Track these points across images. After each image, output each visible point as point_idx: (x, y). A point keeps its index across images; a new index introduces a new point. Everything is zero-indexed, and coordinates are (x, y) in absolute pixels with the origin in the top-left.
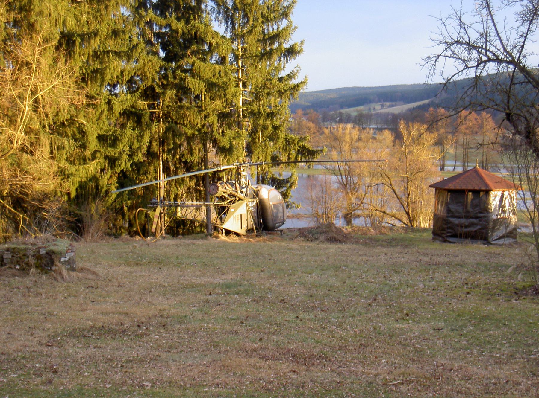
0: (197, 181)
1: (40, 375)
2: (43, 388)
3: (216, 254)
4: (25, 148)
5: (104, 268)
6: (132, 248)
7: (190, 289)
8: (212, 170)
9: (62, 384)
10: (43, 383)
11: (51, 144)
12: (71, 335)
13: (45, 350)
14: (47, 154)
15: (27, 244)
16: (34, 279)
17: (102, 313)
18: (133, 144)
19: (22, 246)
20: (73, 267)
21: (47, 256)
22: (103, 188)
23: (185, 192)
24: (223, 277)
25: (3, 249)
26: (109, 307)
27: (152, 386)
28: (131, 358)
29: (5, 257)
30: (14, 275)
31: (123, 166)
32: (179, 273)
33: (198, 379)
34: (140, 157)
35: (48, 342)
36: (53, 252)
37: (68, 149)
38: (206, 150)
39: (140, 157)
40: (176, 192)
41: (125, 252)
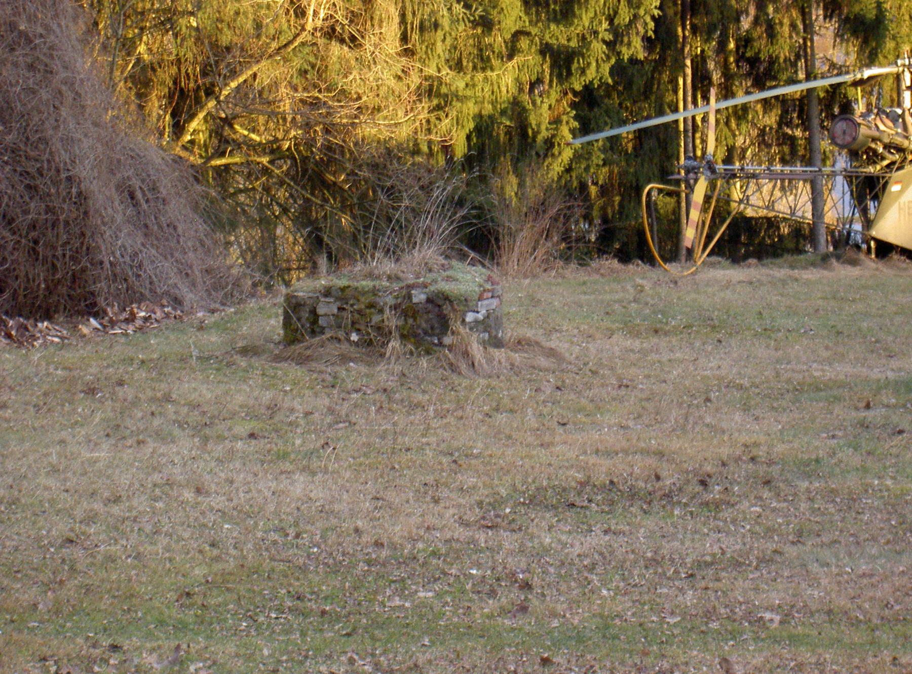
0: (785, 112)
1: (492, 593)
2: (507, 622)
3: (860, 307)
4: (338, 29)
5: (572, 343)
6: (632, 290)
7: (812, 395)
8: (826, 82)
9: (554, 615)
10: (503, 612)
11: (403, 16)
12: (536, 501)
13: (482, 537)
14: (392, 45)
15: (378, 277)
16: (398, 368)
17: (597, 452)
18: (616, 13)
19: (364, 283)
20: (496, 337)
21: (430, 306)
22: (538, 132)
23: (752, 144)
24: (894, 363)
25: (315, 291)
26: (611, 438)
27: (781, 622)
28: (708, 559)
29: (321, 310)
30: (344, 359)
31: (591, 73)
32: (773, 353)
33: (897, 607)
34: (636, 48)
35: (483, 518)
36: (447, 298)
37: (447, 28)
38: (808, 28)
39: (636, 48)
40: (730, 142)
41: (620, 301)
